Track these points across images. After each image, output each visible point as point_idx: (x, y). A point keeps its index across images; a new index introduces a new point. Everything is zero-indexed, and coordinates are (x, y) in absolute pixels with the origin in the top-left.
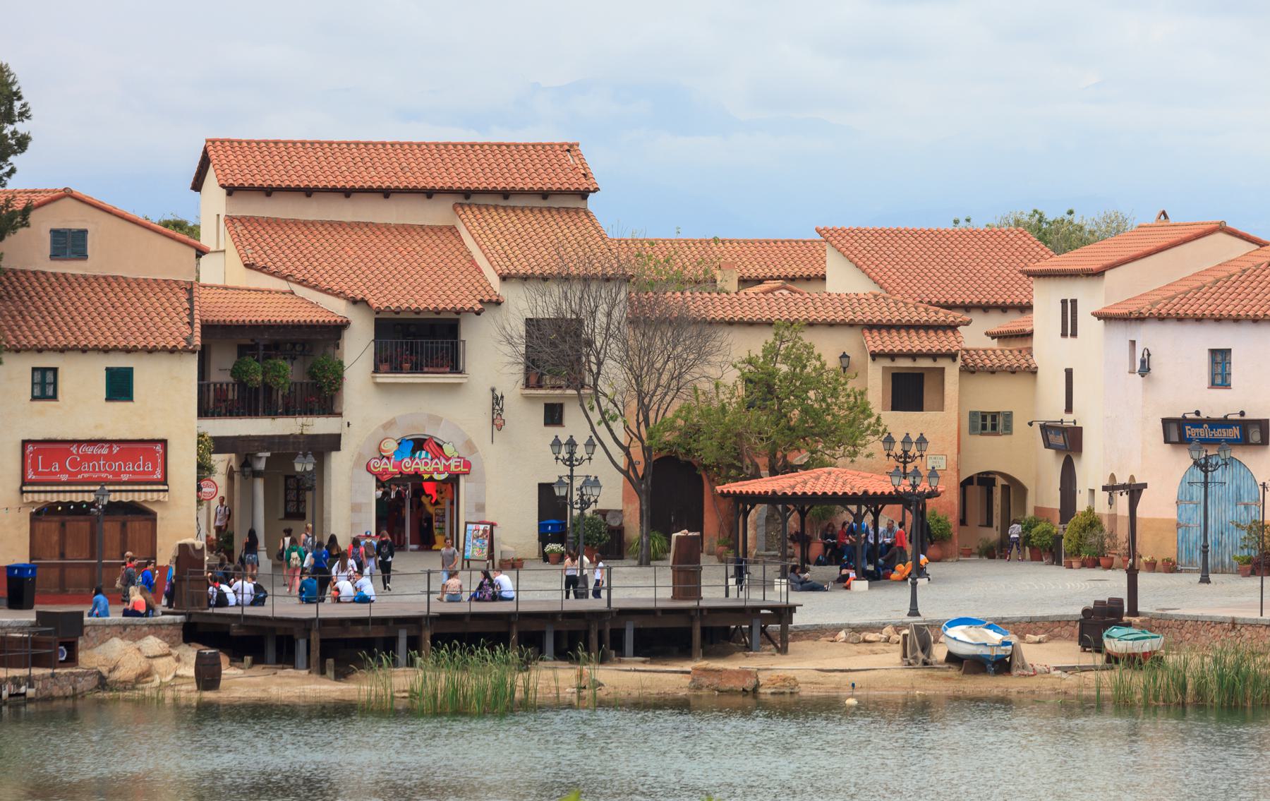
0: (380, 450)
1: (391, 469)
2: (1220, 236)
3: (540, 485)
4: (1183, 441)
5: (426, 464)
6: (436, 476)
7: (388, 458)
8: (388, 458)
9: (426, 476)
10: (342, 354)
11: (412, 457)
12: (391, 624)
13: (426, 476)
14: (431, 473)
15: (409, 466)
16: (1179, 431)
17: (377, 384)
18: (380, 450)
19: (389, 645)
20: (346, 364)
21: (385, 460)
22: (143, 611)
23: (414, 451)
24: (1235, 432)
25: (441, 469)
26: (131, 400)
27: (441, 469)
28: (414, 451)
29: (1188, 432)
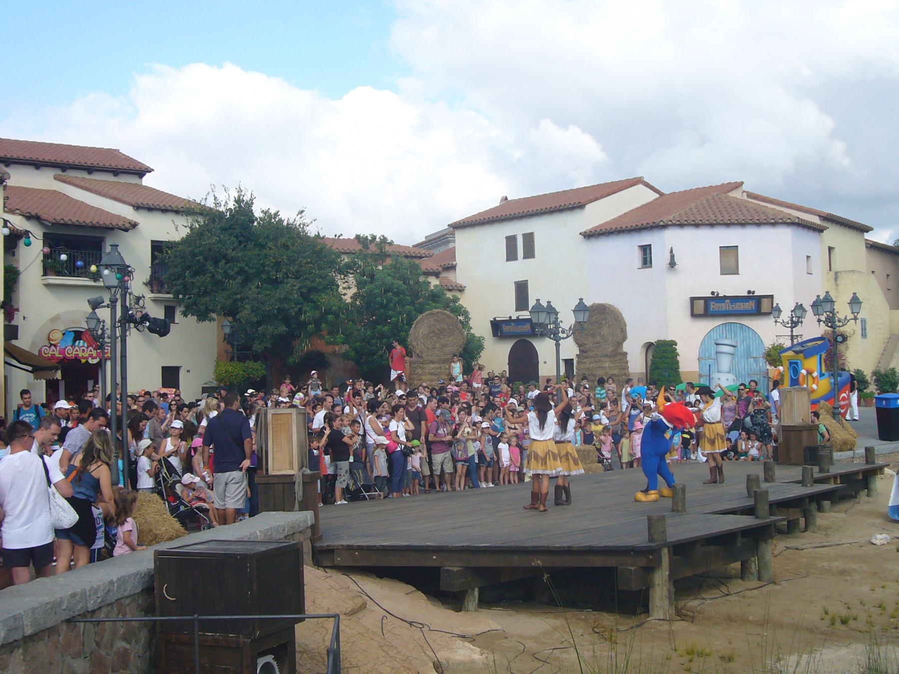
0: (49, 339)
1: (57, 355)
2: (640, 186)
3: (164, 369)
4: (707, 314)
5: (83, 351)
6: (91, 361)
7: (55, 346)
8: (55, 346)
9: (83, 361)
10: (18, 261)
11: (73, 346)
12: (740, 541)
13: (83, 361)
14: (87, 358)
15: (71, 353)
16: (706, 307)
17: (48, 286)
18: (49, 339)
19: (558, 574)
20: (21, 269)
21: (53, 348)
22: (318, 544)
23: (75, 340)
24: (750, 306)
25: (95, 355)
26: (152, 241)
27: (95, 355)
28: (75, 340)
29: (712, 307)
